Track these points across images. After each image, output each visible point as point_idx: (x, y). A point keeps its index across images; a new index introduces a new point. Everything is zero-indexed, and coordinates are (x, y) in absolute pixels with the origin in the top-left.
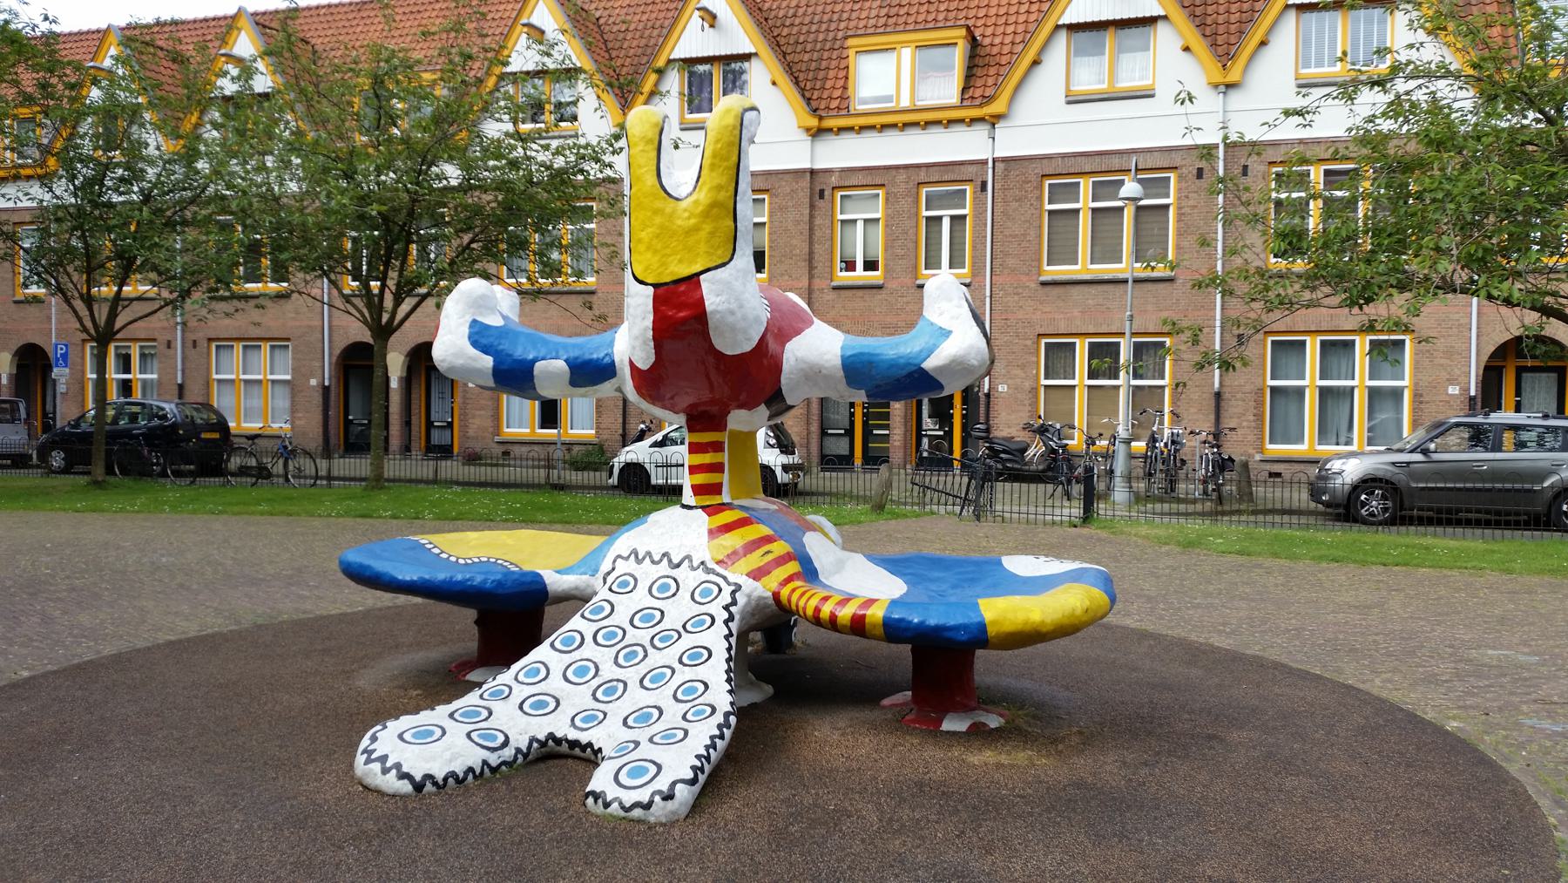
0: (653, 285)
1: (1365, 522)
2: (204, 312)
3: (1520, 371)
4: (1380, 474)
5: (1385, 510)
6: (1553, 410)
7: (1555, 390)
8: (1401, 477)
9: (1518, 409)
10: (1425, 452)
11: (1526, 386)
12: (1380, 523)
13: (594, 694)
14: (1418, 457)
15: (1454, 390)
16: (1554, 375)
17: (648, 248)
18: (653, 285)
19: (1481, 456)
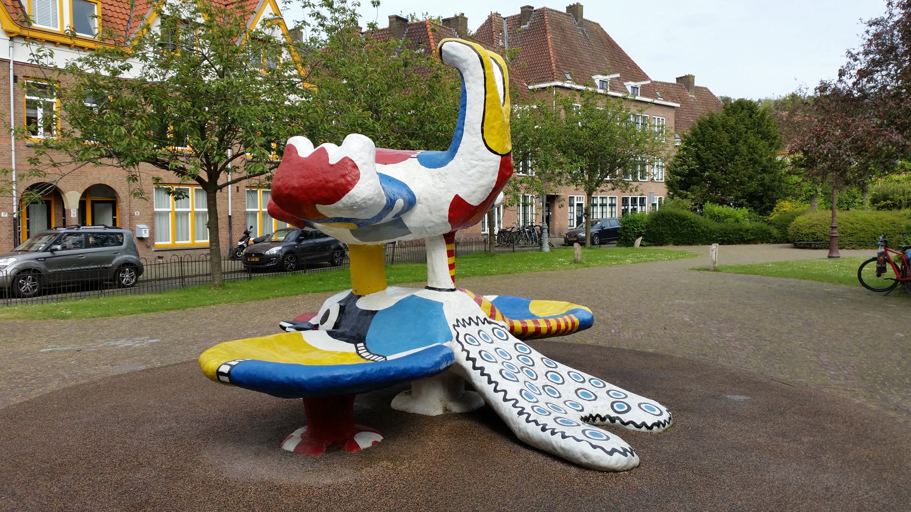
0: (502, 156)
1: (124, 286)
2: (592, 125)
3: (93, 203)
4: (28, 266)
5: (34, 288)
6: (110, 224)
7: (45, 214)
8: (41, 266)
9: (93, 224)
10: (52, 251)
11: (31, 212)
12: (35, 295)
13: (547, 373)
14: (48, 254)
15: (4, 215)
16: (96, 205)
17: (498, 133)
18: (502, 156)
19: (886, 215)
